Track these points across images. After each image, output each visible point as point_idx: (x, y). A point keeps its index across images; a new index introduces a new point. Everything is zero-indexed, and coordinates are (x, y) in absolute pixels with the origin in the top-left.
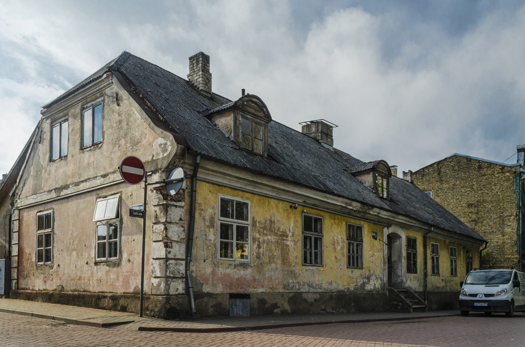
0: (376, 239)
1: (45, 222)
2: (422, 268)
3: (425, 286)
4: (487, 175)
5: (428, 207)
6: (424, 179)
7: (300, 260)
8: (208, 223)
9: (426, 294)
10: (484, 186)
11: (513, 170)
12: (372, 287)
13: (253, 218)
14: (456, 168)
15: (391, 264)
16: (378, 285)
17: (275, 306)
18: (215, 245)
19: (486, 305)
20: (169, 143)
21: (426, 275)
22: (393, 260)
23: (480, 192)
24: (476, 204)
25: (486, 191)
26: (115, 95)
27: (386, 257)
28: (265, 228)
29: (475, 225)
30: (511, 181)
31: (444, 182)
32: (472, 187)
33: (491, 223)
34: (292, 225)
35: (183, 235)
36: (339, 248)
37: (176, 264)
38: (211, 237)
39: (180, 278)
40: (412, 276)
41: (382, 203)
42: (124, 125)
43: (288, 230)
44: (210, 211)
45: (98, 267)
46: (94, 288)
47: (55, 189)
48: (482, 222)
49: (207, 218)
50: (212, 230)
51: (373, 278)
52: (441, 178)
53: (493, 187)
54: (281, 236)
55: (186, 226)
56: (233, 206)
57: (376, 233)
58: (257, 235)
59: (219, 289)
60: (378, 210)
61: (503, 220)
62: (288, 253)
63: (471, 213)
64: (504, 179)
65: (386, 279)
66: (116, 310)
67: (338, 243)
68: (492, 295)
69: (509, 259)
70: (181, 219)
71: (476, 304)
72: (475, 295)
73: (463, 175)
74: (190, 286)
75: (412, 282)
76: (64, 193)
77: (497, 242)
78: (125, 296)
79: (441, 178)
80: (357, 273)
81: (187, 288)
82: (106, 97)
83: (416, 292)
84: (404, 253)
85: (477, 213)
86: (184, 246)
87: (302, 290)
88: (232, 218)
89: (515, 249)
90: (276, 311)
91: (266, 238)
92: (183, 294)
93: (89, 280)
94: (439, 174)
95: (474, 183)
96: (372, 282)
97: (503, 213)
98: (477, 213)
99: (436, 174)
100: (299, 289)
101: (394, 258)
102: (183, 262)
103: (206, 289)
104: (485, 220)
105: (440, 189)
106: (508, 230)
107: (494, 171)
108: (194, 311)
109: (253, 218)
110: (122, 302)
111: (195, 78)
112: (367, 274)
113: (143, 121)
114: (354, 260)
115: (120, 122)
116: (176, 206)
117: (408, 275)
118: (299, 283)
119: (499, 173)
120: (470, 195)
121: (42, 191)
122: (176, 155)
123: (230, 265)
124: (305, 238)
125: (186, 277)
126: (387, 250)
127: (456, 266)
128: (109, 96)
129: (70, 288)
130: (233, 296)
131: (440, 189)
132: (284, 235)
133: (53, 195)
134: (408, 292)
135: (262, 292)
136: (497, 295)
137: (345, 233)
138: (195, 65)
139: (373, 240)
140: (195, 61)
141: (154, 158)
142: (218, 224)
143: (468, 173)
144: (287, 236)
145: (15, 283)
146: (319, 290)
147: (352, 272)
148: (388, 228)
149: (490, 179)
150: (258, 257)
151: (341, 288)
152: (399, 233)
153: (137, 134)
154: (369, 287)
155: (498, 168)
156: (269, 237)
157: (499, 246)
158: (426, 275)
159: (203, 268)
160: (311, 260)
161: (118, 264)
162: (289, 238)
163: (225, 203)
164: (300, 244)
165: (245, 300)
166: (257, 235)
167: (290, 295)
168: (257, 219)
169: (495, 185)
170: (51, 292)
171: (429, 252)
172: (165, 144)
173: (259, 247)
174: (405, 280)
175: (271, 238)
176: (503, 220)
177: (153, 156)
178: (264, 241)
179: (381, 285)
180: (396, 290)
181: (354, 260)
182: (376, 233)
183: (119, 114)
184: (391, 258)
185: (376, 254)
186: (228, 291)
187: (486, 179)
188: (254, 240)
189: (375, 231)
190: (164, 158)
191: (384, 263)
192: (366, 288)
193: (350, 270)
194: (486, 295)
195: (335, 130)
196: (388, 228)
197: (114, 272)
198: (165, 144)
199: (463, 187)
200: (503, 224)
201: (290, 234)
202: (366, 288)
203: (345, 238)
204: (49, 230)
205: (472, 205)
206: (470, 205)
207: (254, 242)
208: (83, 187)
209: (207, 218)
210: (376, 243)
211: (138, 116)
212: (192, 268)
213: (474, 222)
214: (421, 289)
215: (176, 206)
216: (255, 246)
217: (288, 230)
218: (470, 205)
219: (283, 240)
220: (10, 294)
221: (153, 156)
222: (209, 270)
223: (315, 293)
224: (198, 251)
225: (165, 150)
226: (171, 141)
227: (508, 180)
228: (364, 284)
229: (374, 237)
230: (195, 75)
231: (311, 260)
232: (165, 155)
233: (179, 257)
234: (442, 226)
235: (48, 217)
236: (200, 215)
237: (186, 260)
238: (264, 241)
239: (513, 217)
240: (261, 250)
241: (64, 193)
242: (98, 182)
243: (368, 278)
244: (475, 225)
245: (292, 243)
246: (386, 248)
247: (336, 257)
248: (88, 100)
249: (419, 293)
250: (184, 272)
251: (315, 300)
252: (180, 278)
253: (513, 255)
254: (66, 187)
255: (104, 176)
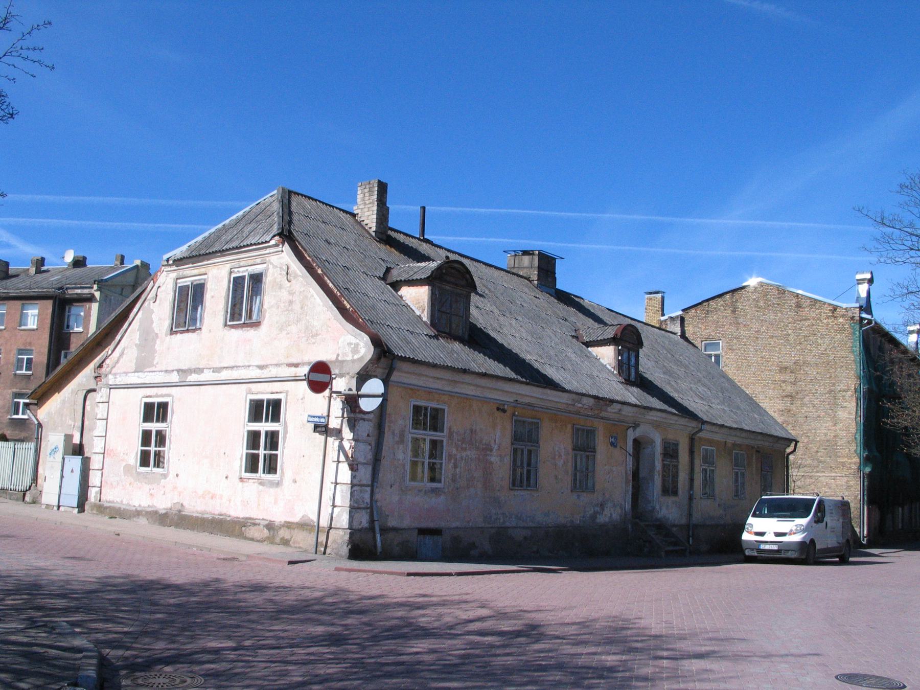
0: (616, 446)
1: (156, 411)
2: (687, 488)
3: (690, 515)
4: (809, 319)
5: (704, 385)
6: (710, 318)
7: (506, 483)
8: (397, 439)
9: (690, 528)
10: (805, 337)
11: (850, 314)
12: (607, 520)
13: (450, 429)
14: (761, 303)
15: (637, 481)
16: (616, 516)
17: (473, 546)
18: (404, 465)
19: (775, 547)
20: (362, 344)
21: (691, 498)
22: (641, 476)
23: (798, 347)
24: (793, 367)
25: (809, 347)
26: (285, 268)
27: (630, 473)
28: (463, 440)
29: (792, 404)
30: (847, 333)
31: (742, 326)
32: (786, 337)
33: (816, 401)
34: (498, 434)
35: (370, 456)
36: (560, 463)
37: (361, 491)
38: (400, 456)
39: (364, 508)
40: (671, 499)
41: (626, 393)
42: (297, 307)
43: (492, 442)
44: (400, 422)
45: (245, 484)
46: (236, 511)
47: (178, 371)
48: (802, 399)
49: (397, 432)
50: (401, 446)
51: (609, 505)
52: (736, 318)
53: (820, 341)
54: (483, 449)
55: (373, 443)
56: (425, 415)
57: (616, 438)
58: (454, 451)
59: (406, 523)
60: (619, 406)
61: (834, 397)
62: (491, 474)
63: (784, 382)
64: (836, 327)
65: (628, 506)
66: (272, 543)
67: (560, 456)
68: (784, 534)
69: (843, 464)
70: (368, 435)
71: (763, 547)
72: (762, 534)
73: (772, 317)
74: (376, 518)
75: (669, 510)
76: (193, 378)
77: (826, 435)
78: (288, 525)
79: (736, 318)
80: (585, 498)
81: (372, 521)
82: (271, 266)
83: (674, 526)
84: (658, 466)
85: (794, 383)
86: (370, 468)
87: (508, 524)
88: (425, 429)
89: (853, 448)
90: (472, 552)
91: (464, 454)
92: (366, 528)
93: (230, 501)
94: (734, 312)
95: (790, 332)
96: (607, 512)
97: (834, 385)
98: (794, 383)
99: (729, 311)
100: (504, 522)
101: (643, 473)
102: (369, 489)
103: (392, 523)
104: (807, 395)
105: (736, 338)
106: (842, 414)
107: (820, 314)
108: (379, 549)
109: (450, 429)
110: (284, 533)
111: (366, 214)
112: (600, 499)
113: (325, 309)
114: (582, 481)
115: (291, 302)
116: (364, 420)
117: (662, 499)
118: (504, 514)
119: (828, 317)
120: (783, 351)
121: (153, 369)
122: (370, 360)
123: (420, 491)
124: (515, 450)
125: (371, 508)
126: (631, 463)
127: (743, 484)
128: (275, 267)
129: (195, 507)
130: (423, 532)
131: (736, 338)
132: (488, 448)
133: (175, 378)
134: (661, 527)
135: (457, 528)
136: (790, 534)
137: (570, 441)
138: (367, 194)
139: (612, 448)
140: (366, 190)
141: (340, 358)
142: (409, 437)
143: (779, 314)
144: (491, 450)
145: (96, 493)
146: (531, 525)
147: (578, 496)
148: (634, 430)
149: (814, 327)
150: (454, 480)
151: (562, 520)
152: (651, 436)
153: (316, 323)
154: (602, 519)
155: (827, 310)
156: (469, 453)
157: (828, 441)
158: (691, 498)
159: (388, 497)
160: (521, 482)
161: (278, 484)
162: (494, 452)
163: (417, 409)
164: (508, 460)
165: (436, 537)
166: (454, 451)
167: (493, 531)
168: (455, 429)
169: (822, 337)
170: (164, 512)
171: (698, 462)
172: (357, 345)
173: (455, 466)
174: (657, 507)
175: (471, 454)
176: (834, 397)
177: (338, 355)
178: (462, 458)
179: (621, 516)
180: (642, 524)
181: (582, 481)
182: (616, 438)
183: (291, 293)
184: (638, 474)
185: (614, 469)
186: (416, 525)
187: (809, 326)
188: (450, 456)
189: (615, 435)
190: (353, 361)
191: (627, 483)
192: (598, 521)
193: (575, 496)
194: (778, 534)
195: (558, 263)
196: (634, 430)
197: (270, 493)
198: (357, 345)
199: (772, 337)
200: (835, 404)
201: (496, 447)
202: (598, 521)
203: (570, 448)
204: (164, 425)
205: (786, 368)
206: (783, 369)
207: (450, 460)
208: (225, 375)
209: (397, 432)
210: (617, 452)
211: (318, 300)
212: (378, 496)
213: (789, 399)
214: (684, 521)
215: (364, 420)
216: (451, 465)
217: (492, 442)
218: (783, 369)
219: (487, 455)
220: (87, 507)
221: (338, 355)
222: (395, 498)
223: (524, 528)
224: (386, 475)
225: (355, 350)
226: (366, 344)
227: (842, 330)
228: (596, 513)
229: (612, 444)
230: (366, 210)
231: (521, 482)
232: (356, 357)
233: (364, 482)
234: (720, 422)
235: (163, 406)
236: (389, 427)
237: (372, 486)
238: (462, 458)
239: (849, 393)
240: (458, 470)
241: (193, 378)
242: (255, 373)
243: (602, 505)
244: (792, 404)
245: (498, 459)
246: (630, 461)
247: (556, 477)
248: (242, 264)
249: (680, 526)
250: (368, 500)
251: (525, 538)
252: (364, 508)
253: (850, 458)
254: (199, 371)
255: (261, 367)
